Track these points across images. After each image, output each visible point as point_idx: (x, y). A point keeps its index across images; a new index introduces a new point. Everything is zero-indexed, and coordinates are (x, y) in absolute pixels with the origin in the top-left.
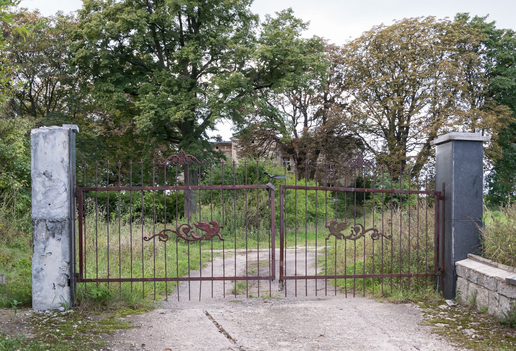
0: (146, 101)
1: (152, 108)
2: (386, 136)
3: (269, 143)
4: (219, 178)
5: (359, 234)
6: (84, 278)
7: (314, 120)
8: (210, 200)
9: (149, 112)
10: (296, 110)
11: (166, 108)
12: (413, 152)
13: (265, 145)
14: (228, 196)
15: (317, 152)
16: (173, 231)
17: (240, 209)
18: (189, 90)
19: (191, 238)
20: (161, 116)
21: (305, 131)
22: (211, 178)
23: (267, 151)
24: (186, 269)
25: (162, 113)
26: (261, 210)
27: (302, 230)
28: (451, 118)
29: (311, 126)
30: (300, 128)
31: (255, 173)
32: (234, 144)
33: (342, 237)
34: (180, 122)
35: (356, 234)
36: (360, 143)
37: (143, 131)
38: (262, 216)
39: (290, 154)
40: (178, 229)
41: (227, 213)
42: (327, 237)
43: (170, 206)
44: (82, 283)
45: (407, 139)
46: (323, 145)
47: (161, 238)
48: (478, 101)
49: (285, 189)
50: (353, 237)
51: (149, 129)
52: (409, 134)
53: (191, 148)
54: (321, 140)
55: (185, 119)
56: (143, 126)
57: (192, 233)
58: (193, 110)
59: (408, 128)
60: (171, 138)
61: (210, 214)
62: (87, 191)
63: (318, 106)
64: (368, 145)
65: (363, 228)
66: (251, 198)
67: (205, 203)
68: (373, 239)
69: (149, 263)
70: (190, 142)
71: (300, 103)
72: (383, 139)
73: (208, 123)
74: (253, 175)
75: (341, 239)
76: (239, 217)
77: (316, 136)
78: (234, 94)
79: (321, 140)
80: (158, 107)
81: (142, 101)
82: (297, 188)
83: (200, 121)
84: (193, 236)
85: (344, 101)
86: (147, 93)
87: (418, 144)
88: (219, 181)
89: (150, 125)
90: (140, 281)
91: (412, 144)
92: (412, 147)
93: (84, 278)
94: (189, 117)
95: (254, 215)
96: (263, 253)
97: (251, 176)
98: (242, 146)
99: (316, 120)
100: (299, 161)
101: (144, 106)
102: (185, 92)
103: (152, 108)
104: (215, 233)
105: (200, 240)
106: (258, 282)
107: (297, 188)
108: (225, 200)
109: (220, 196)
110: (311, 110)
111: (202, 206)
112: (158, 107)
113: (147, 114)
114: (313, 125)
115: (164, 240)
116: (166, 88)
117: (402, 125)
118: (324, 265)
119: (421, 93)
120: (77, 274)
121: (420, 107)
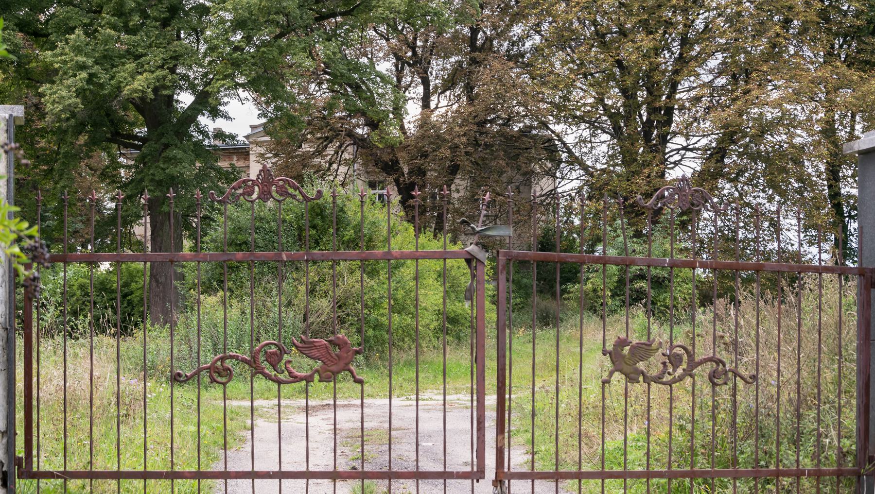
0: (67, 50)
1: (83, 67)
2: (617, 133)
3: (340, 147)
4: (240, 230)
5: (679, 371)
6: (35, 469)
7: (443, 92)
8: (221, 282)
9: (75, 76)
10: (402, 69)
11: (113, 66)
12: (684, 168)
13: (330, 151)
14: (263, 274)
15: (454, 170)
16: (244, 361)
17: (289, 304)
18: (165, 23)
20: (101, 86)
21: (424, 123)
22: (219, 231)
23: (335, 166)
25: (104, 77)
26: (340, 307)
27: (431, 356)
28: (776, 87)
29: (437, 108)
30: (413, 110)
32: (255, 150)
33: (641, 378)
34: (143, 99)
35: (674, 371)
36: (551, 149)
37: (60, 120)
38: (342, 321)
39: (388, 174)
40: (254, 357)
41: (259, 313)
42: (605, 376)
44: (28, 482)
45: (669, 137)
46: (467, 153)
47: (215, 375)
48: (841, 46)
49: (394, 262)
50: (667, 378)
51: (73, 115)
52: (673, 125)
53: (168, 160)
55: (156, 90)
56: (60, 107)
57: (289, 366)
58: (173, 71)
59: (669, 111)
60: (120, 137)
61: (220, 314)
62: (757, 271)
63: (453, 59)
64: (569, 151)
65: (691, 356)
66: (316, 279)
67: (208, 290)
68: (714, 385)
69: (131, 433)
70: (167, 146)
71: (415, 53)
72: (605, 137)
73: (207, 102)
74: (321, 227)
75: (638, 382)
76: (289, 322)
77: (450, 130)
78: (265, 35)
79: (464, 139)
80: (96, 63)
81: (58, 51)
82: (416, 257)
83: (185, 99)
84: (290, 373)
85: (515, 48)
86: (71, 30)
87: (691, 150)
89: (77, 104)
90: (166, 478)
91: (679, 150)
92: (677, 158)
93: (35, 469)
94: (165, 87)
95: (323, 318)
97: (314, 227)
98: (276, 155)
99: (448, 93)
100: (406, 191)
101: (65, 62)
102: (156, 28)
103: (83, 67)
104: (342, 364)
106: (445, 484)
107: (416, 257)
108: (255, 281)
109: (244, 273)
110: (438, 68)
111: (202, 297)
112: (96, 63)
113: (70, 81)
114: (444, 105)
115: (224, 380)
116: (113, 19)
117: (657, 105)
118: (527, 442)
119: (702, 26)
120: (20, 459)
121: (700, 60)
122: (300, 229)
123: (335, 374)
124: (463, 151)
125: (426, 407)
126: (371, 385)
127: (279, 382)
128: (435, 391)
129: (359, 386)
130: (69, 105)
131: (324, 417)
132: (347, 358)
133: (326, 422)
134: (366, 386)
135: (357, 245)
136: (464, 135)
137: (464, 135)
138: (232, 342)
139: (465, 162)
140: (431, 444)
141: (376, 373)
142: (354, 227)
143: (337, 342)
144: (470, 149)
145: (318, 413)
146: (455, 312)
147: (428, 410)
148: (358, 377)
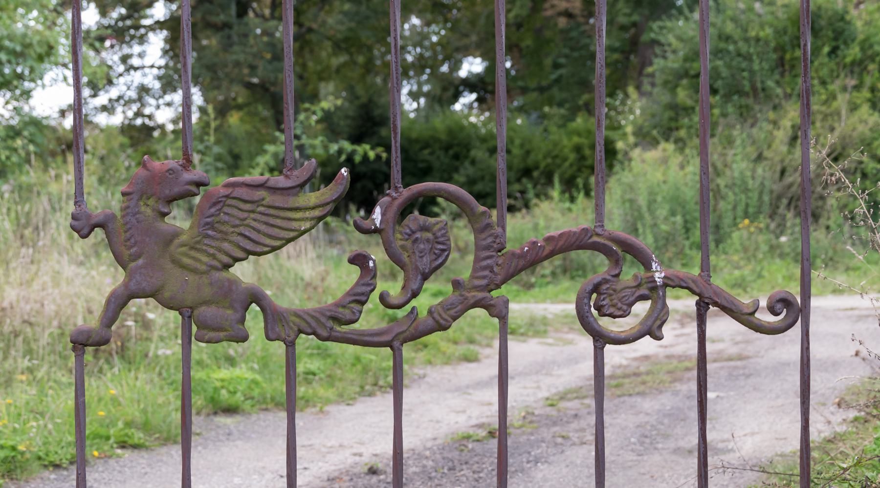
135: (865, 68)
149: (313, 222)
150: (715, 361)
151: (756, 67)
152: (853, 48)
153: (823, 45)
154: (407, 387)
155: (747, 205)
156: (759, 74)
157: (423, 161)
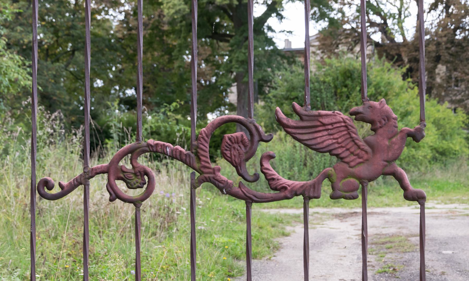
4: (292, 88)
19: (261, 188)
24: (238, 258)
31: (353, 80)
43: (215, 139)
46: (447, 48)
47: (121, 186)
54: (445, 39)
57: (267, 165)
84: (270, 180)
88: (294, 94)
96: (381, 217)
97: (346, 86)
105: (307, 199)
122: (336, 87)
123: (364, 181)
124: (444, 47)
125: (434, 215)
126: (388, 197)
127: (250, 200)
128: (436, 202)
129: (416, 205)
130: (180, 10)
131: (353, 223)
132: (389, 147)
133: (353, 227)
134: (428, 204)
135: (376, 98)
136: (445, 36)
137: (445, 36)
138: (286, 167)
139: (445, 56)
140: (450, 252)
141: (391, 188)
142: (375, 86)
143: (369, 114)
144: (449, 45)
145: (347, 219)
146: (442, 148)
147: (436, 218)
148: (412, 187)
149: (321, 124)
150: (372, 227)
151: (324, 96)
152: (371, 88)
153: (356, 86)
154: (310, 207)
155: (325, 164)
156: (325, 99)
157: (461, 85)
